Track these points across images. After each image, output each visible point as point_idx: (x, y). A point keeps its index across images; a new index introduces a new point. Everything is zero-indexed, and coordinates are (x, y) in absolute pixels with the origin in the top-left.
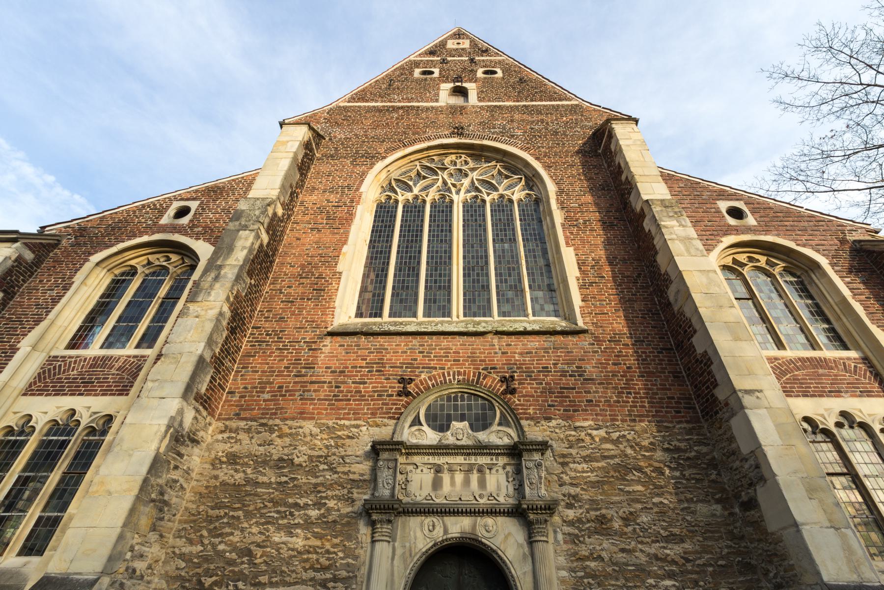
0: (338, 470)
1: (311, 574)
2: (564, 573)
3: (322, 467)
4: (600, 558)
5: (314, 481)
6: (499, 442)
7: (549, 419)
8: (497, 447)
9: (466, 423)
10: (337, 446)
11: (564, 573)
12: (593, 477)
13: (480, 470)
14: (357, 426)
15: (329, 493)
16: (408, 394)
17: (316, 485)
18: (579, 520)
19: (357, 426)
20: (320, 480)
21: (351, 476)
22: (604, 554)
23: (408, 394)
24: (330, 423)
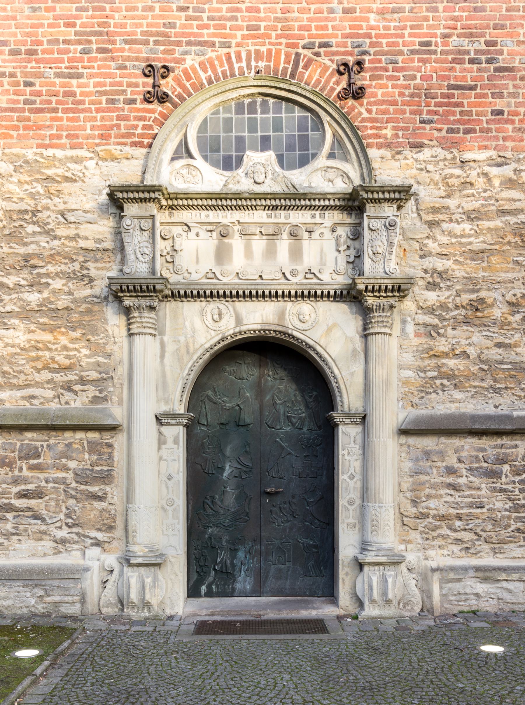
0: (59, 233)
1: (46, 375)
2: (409, 374)
3: (31, 229)
4: (465, 355)
5: (22, 250)
6: (328, 188)
7: (418, 146)
8: (324, 196)
9: (270, 155)
10: (49, 195)
11: (409, 374)
12: (477, 244)
13: (293, 235)
14: (79, 160)
15: (51, 268)
16: (163, 98)
17: (27, 258)
18: (443, 306)
19: (79, 160)
20: (31, 249)
21: (82, 244)
22: (472, 351)
23: (163, 98)
24: (30, 154)
